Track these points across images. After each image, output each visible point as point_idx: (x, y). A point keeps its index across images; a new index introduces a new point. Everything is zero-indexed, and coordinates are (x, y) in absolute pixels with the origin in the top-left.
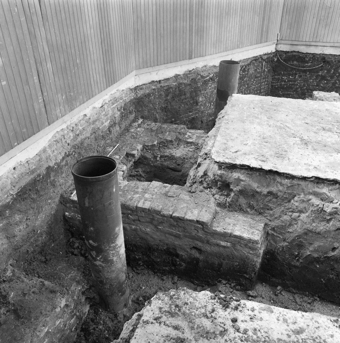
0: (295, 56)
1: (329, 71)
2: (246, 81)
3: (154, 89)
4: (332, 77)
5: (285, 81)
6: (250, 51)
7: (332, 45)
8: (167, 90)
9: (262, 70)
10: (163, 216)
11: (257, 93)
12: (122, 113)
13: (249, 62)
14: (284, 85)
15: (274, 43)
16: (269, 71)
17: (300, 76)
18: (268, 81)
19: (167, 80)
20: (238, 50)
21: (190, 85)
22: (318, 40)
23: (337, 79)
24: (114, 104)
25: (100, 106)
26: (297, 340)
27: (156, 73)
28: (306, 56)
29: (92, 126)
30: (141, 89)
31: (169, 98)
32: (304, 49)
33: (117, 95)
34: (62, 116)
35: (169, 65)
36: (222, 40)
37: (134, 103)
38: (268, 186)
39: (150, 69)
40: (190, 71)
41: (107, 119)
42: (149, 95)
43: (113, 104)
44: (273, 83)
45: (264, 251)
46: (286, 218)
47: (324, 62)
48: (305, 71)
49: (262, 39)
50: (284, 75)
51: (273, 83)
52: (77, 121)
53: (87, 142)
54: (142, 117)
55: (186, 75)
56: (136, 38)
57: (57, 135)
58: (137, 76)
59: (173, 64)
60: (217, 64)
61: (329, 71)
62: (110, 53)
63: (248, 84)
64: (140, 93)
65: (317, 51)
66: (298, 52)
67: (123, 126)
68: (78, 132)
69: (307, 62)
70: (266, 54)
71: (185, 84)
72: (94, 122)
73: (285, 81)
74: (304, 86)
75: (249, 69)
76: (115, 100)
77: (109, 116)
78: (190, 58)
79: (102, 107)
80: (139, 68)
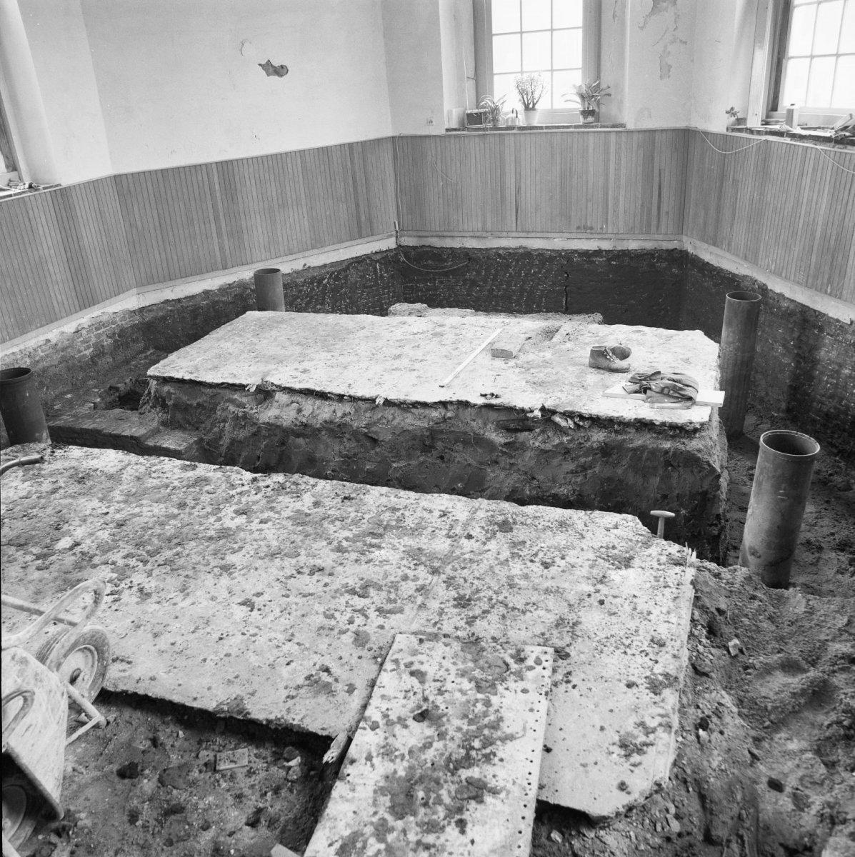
0: (427, 252)
1: (479, 273)
2: (345, 293)
3: (171, 311)
4: (485, 281)
5: (422, 291)
6: (341, 251)
7: (472, 234)
8: (193, 311)
9: (376, 276)
10: (104, 435)
11: (375, 311)
12: (116, 341)
13: (344, 266)
14: (422, 296)
15: (391, 236)
16: (392, 277)
17: (442, 282)
18: (394, 292)
19: (192, 297)
20: (316, 251)
21: (231, 303)
22: (451, 228)
23: (492, 285)
24: (99, 329)
25: (74, 331)
26: (483, 704)
27: (171, 289)
28: (442, 252)
29: (62, 354)
30: (150, 311)
31: (198, 321)
32: (437, 243)
33: (105, 318)
34: (10, 339)
35: (190, 279)
36: (280, 239)
37: (139, 329)
38: (196, 398)
39: (160, 285)
40: (229, 284)
41: (88, 347)
42: (164, 318)
43: (97, 329)
44: (406, 294)
45: (137, 435)
46: (216, 429)
47: (469, 259)
48: (446, 274)
49: (361, 230)
50: (418, 281)
51: (406, 294)
52: (35, 346)
53: (51, 371)
54: (156, 348)
55: (224, 290)
56: (132, 249)
57: (6, 358)
58: (141, 296)
59: (198, 277)
60: (252, 274)
61: (479, 273)
62: (83, 270)
63: (350, 298)
64: (148, 317)
65: (456, 244)
66: (429, 246)
67: (120, 357)
68: (37, 359)
69: (446, 261)
70: (376, 253)
71: (223, 302)
72: (63, 349)
73: (422, 291)
74: (450, 296)
75: (347, 276)
76: (99, 325)
77: (91, 343)
78: (225, 268)
79: (77, 332)
80: (140, 284)
